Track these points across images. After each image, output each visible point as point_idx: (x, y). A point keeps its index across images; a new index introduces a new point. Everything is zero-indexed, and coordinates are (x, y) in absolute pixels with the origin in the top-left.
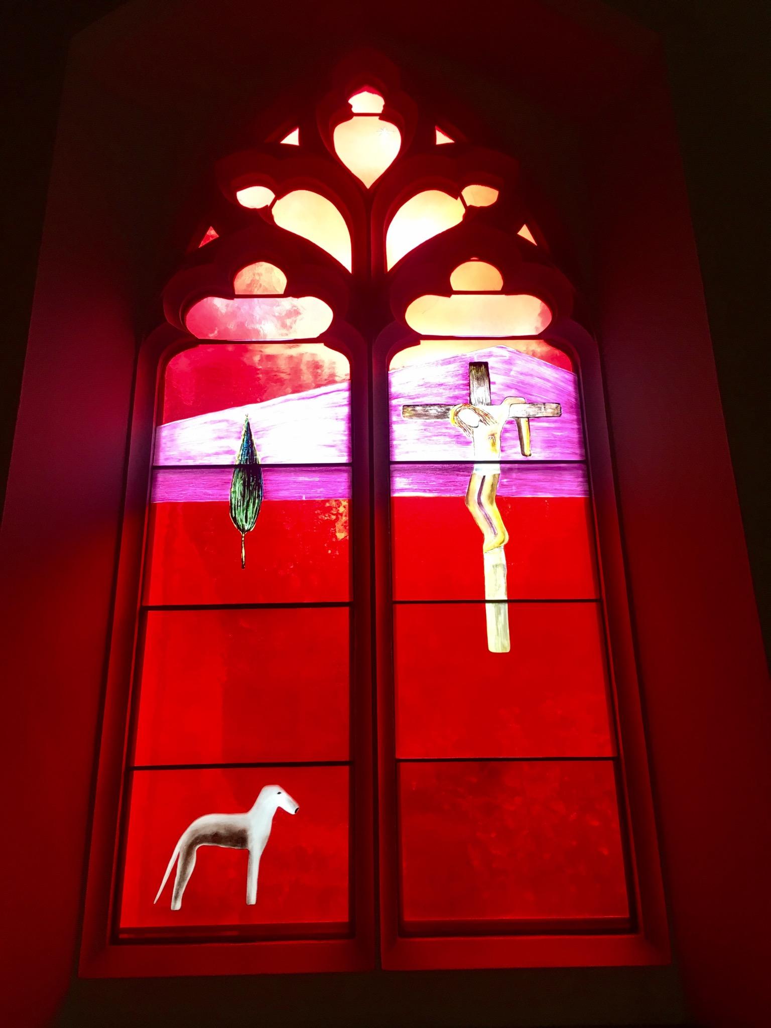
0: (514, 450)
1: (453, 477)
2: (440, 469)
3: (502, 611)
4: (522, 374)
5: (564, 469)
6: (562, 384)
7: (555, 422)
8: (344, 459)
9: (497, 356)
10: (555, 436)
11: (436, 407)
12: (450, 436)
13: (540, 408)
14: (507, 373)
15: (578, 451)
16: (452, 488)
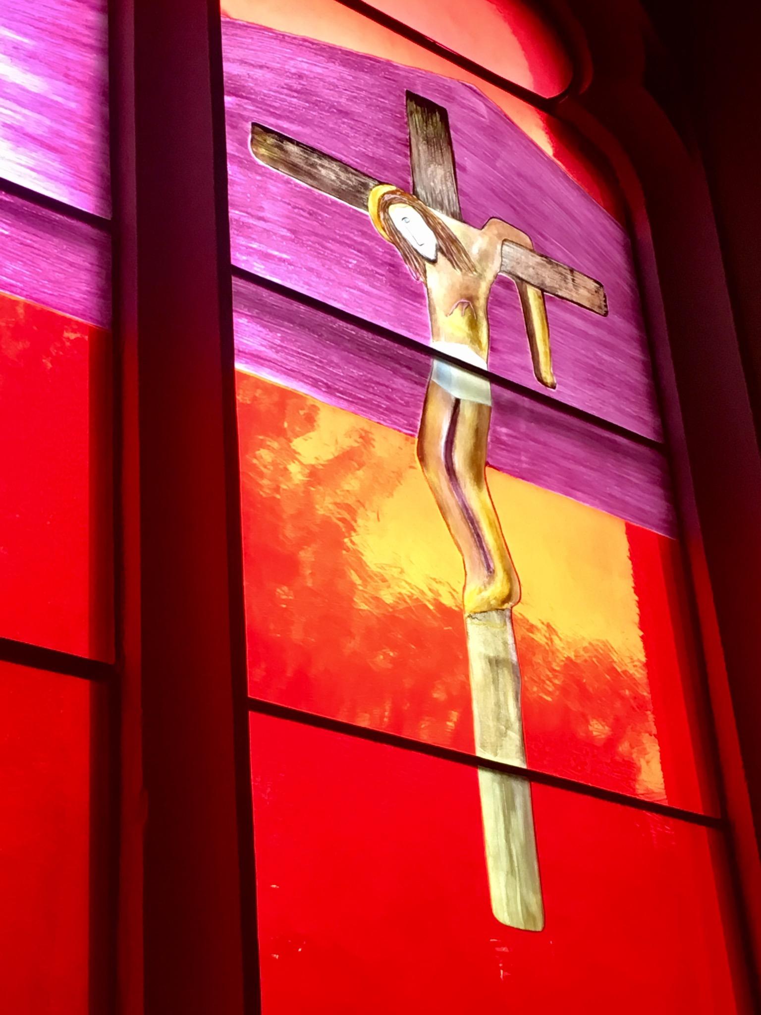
0: (516, 359)
1: (382, 374)
2: (352, 340)
3: (519, 801)
4: (519, 175)
5: (626, 453)
6: (600, 238)
7: (596, 324)
8: (82, 199)
9: (463, 106)
10: (601, 361)
11: (335, 166)
12: (370, 255)
13: (565, 279)
14: (491, 158)
15: (648, 417)
16: (385, 403)
